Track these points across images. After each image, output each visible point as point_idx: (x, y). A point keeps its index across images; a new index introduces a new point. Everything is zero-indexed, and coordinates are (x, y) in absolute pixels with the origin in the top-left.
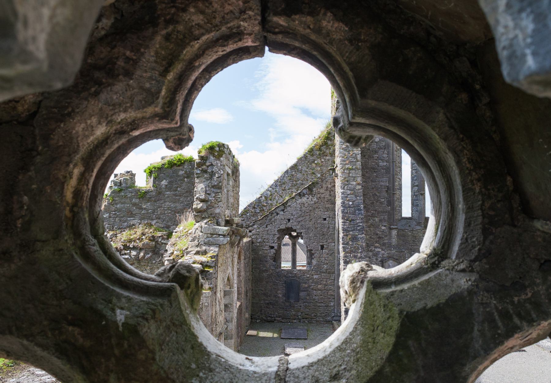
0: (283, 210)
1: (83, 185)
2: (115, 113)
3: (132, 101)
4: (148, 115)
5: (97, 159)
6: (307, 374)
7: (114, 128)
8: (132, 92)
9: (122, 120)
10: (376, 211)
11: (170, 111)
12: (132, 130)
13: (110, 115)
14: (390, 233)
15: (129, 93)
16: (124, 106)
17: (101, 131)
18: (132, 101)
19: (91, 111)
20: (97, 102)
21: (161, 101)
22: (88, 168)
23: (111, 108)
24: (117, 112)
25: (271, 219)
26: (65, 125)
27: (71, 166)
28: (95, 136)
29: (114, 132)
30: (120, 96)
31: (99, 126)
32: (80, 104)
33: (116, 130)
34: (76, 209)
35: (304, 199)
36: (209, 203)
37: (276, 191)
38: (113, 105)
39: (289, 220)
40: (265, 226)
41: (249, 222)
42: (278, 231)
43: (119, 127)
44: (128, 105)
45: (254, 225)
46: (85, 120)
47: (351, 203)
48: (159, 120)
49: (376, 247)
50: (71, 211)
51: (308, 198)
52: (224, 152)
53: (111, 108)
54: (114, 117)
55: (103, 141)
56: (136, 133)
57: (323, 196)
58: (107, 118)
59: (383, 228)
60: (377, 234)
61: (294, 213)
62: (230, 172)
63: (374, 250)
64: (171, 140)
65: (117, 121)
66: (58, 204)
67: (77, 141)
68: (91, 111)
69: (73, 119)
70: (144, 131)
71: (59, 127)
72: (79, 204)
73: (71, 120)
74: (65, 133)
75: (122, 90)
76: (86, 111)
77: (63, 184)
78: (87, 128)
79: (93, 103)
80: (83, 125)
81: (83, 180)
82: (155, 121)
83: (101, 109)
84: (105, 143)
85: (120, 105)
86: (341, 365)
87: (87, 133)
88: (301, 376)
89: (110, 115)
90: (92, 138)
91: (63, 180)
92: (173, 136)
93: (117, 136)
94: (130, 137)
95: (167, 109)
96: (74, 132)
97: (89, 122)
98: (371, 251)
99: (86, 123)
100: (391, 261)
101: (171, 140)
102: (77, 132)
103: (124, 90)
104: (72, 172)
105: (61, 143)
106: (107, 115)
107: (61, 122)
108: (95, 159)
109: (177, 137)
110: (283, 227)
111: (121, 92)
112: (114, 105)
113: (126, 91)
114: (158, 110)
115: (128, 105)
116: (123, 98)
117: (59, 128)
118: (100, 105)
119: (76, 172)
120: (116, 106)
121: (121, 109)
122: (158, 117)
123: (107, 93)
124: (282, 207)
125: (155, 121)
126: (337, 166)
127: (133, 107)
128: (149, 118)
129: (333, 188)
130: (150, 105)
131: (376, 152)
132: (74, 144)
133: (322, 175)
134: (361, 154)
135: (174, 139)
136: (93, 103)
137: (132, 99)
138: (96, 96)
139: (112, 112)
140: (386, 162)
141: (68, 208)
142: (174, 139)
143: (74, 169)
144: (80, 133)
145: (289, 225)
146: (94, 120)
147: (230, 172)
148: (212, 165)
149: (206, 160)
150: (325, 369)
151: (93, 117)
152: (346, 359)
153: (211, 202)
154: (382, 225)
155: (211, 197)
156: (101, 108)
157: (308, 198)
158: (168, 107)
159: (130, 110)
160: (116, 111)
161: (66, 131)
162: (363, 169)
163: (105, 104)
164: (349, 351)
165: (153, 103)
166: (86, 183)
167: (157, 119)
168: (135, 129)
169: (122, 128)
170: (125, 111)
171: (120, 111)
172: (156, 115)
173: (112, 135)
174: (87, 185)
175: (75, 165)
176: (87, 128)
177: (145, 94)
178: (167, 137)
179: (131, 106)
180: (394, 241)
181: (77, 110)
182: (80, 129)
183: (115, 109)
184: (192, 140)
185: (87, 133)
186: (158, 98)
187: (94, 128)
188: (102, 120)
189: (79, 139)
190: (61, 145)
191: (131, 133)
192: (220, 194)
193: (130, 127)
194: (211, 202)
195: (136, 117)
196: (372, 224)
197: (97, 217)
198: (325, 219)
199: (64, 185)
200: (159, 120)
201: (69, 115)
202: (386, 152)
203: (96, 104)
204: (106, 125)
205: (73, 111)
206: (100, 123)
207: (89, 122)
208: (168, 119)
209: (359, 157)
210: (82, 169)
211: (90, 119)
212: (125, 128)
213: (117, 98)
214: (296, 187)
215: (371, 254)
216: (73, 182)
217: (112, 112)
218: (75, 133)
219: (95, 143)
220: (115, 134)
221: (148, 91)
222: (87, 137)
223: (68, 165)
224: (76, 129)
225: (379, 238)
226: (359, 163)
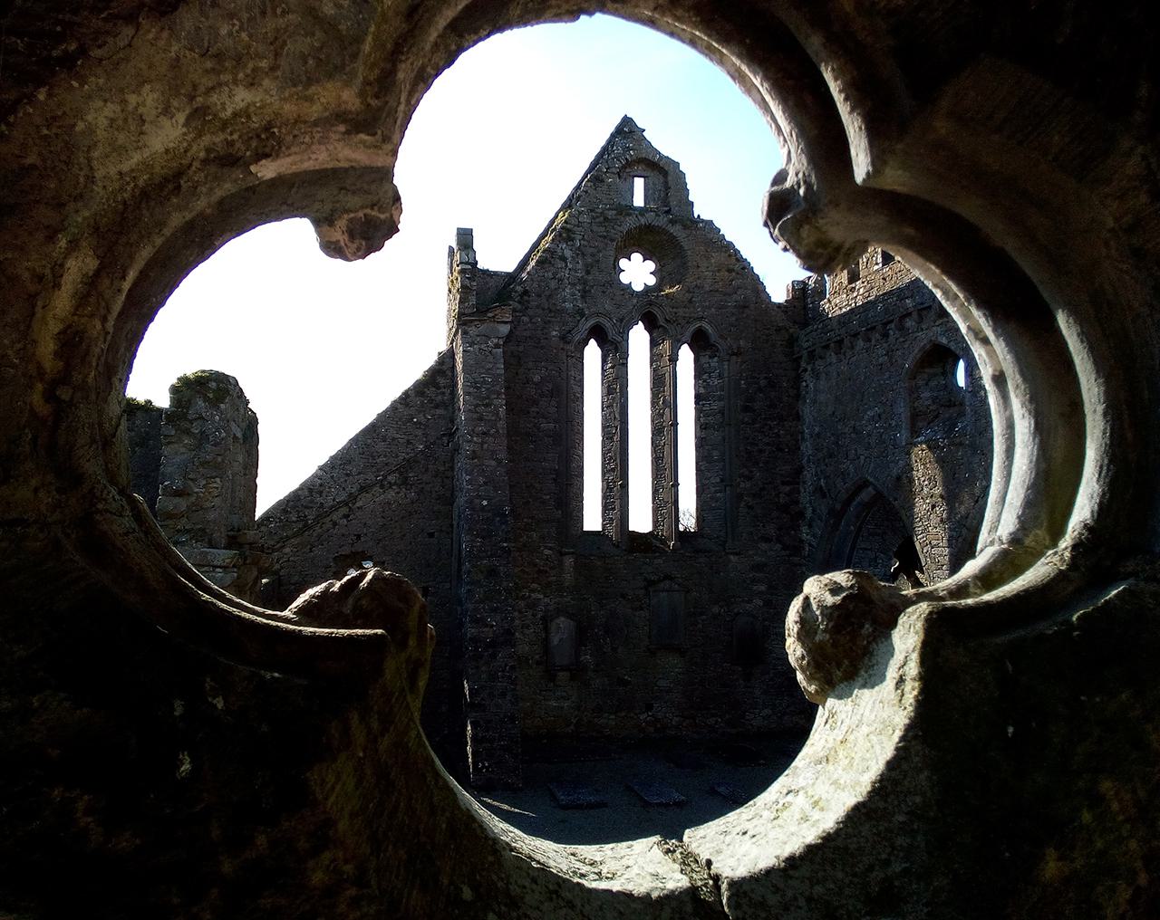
0: (346, 516)
1: (92, 316)
2: (220, 85)
3: (277, 55)
4: (314, 111)
5: (142, 237)
6: (790, 894)
7: (206, 140)
8: (281, 22)
9: (235, 115)
10: (532, 518)
11: (380, 109)
12: (260, 156)
13: (202, 89)
14: (561, 563)
15: (270, 25)
16: (251, 65)
17: (166, 136)
18: (277, 55)
19: (143, 66)
20: (165, 34)
21: (361, 70)
22: (110, 265)
23: (209, 65)
24: (226, 84)
25: (319, 536)
26: (50, 95)
27: (63, 243)
28: (147, 153)
29: (202, 155)
30: (241, 28)
31: (165, 121)
32: (107, 33)
33: (208, 150)
34: (64, 393)
35: (391, 494)
36: (193, 499)
37: (332, 477)
38: (216, 56)
39: (359, 537)
40: (307, 549)
41: (272, 543)
42: (335, 559)
43: (219, 138)
44: (264, 64)
45: (283, 547)
46: (122, 91)
47: (485, 503)
48: (348, 132)
49: (533, 591)
50: (50, 396)
51: (398, 493)
52: (228, 391)
53: (209, 65)
54: (214, 98)
55: (166, 180)
56: (267, 170)
57: (428, 488)
58: (192, 98)
59: (547, 552)
60: (535, 565)
61: (369, 522)
62: (239, 435)
63: (530, 596)
64: (342, 223)
65: (222, 115)
66: (14, 366)
67: (89, 160)
68: (143, 66)
69: (83, 82)
70: (294, 169)
71: (31, 98)
72: (77, 377)
73: (75, 84)
74: (48, 127)
75: (249, 9)
76: (127, 60)
77: (32, 298)
78: (126, 120)
79: (151, 36)
80: (111, 109)
81: (92, 300)
82: (334, 136)
83: (176, 64)
84: (171, 186)
85: (239, 60)
86: (887, 863)
87: (121, 138)
88: (773, 900)
89: (202, 89)
90: (136, 158)
91: (32, 288)
92: (348, 211)
93: (213, 169)
94: (251, 182)
95: (374, 102)
96: (80, 126)
97: (133, 99)
98: (523, 598)
99: (124, 102)
100: (563, 619)
101: (342, 223)
102: (91, 130)
103: (257, 11)
104: (62, 265)
105: (31, 159)
106: (195, 87)
107: (40, 83)
108: (134, 237)
109: (361, 214)
110: (346, 550)
111: (245, 16)
112: (219, 57)
113: (263, 13)
114: (349, 98)
115: (264, 64)
116: (250, 36)
117: (30, 103)
118: (175, 48)
119: (79, 266)
120: (225, 62)
121: (241, 76)
122: (345, 122)
123: (202, 12)
124: (344, 510)
125: (334, 136)
126: (457, 429)
127: (279, 73)
128: (315, 124)
129: (449, 474)
130: (330, 76)
131: (535, 403)
132: (75, 170)
133: (426, 447)
134: (506, 405)
135: (351, 221)
136: (151, 36)
137: (277, 44)
138: (163, 14)
139: (207, 82)
140: (555, 421)
141: (39, 387)
142: (351, 221)
143: (68, 253)
144: (101, 134)
145: (359, 547)
146: (149, 99)
147: (239, 435)
148: (201, 418)
149: (188, 408)
150: (840, 875)
151: (147, 87)
152: (901, 841)
153: (198, 497)
154: (546, 547)
155: (198, 487)
156: (178, 59)
157: (398, 493)
158: (377, 97)
159: (266, 82)
160: (226, 77)
161: (55, 118)
162: (509, 435)
163: (191, 50)
164: (901, 818)
165: (339, 69)
166: (103, 312)
167: (342, 128)
168: (267, 156)
169: (231, 144)
170: (251, 84)
171: (235, 82)
172: (340, 116)
173: (196, 164)
174: (104, 319)
175: (74, 245)
176: (126, 120)
177: (319, 34)
178: (333, 211)
179: (273, 69)
180: (568, 578)
181: (96, 53)
182: (103, 122)
183: (219, 73)
184: (392, 229)
185: (121, 138)
186: (354, 56)
187: (146, 127)
188: (175, 103)
189: (96, 154)
190: (33, 167)
191: (253, 168)
192: (218, 480)
193: (254, 144)
194: (198, 497)
195: (277, 114)
196: (524, 545)
197: (114, 435)
198: (431, 535)
199: (34, 306)
200: (348, 132)
201: (68, 62)
202: (553, 403)
203: (161, 43)
204: (186, 124)
205: (83, 51)
206: (167, 111)
207: (133, 99)
208: (374, 134)
209: (502, 410)
210: (92, 264)
211: (137, 91)
212: (238, 145)
213: (230, 34)
214: (374, 469)
215: (522, 604)
216: (62, 302)
217: (207, 82)
218: (83, 132)
219: (141, 183)
220: (205, 162)
221: (330, 26)
222: (121, 151)
223: (51, 238)
224: (89, 118)
225: (540, 572)
226: (502, 424)
